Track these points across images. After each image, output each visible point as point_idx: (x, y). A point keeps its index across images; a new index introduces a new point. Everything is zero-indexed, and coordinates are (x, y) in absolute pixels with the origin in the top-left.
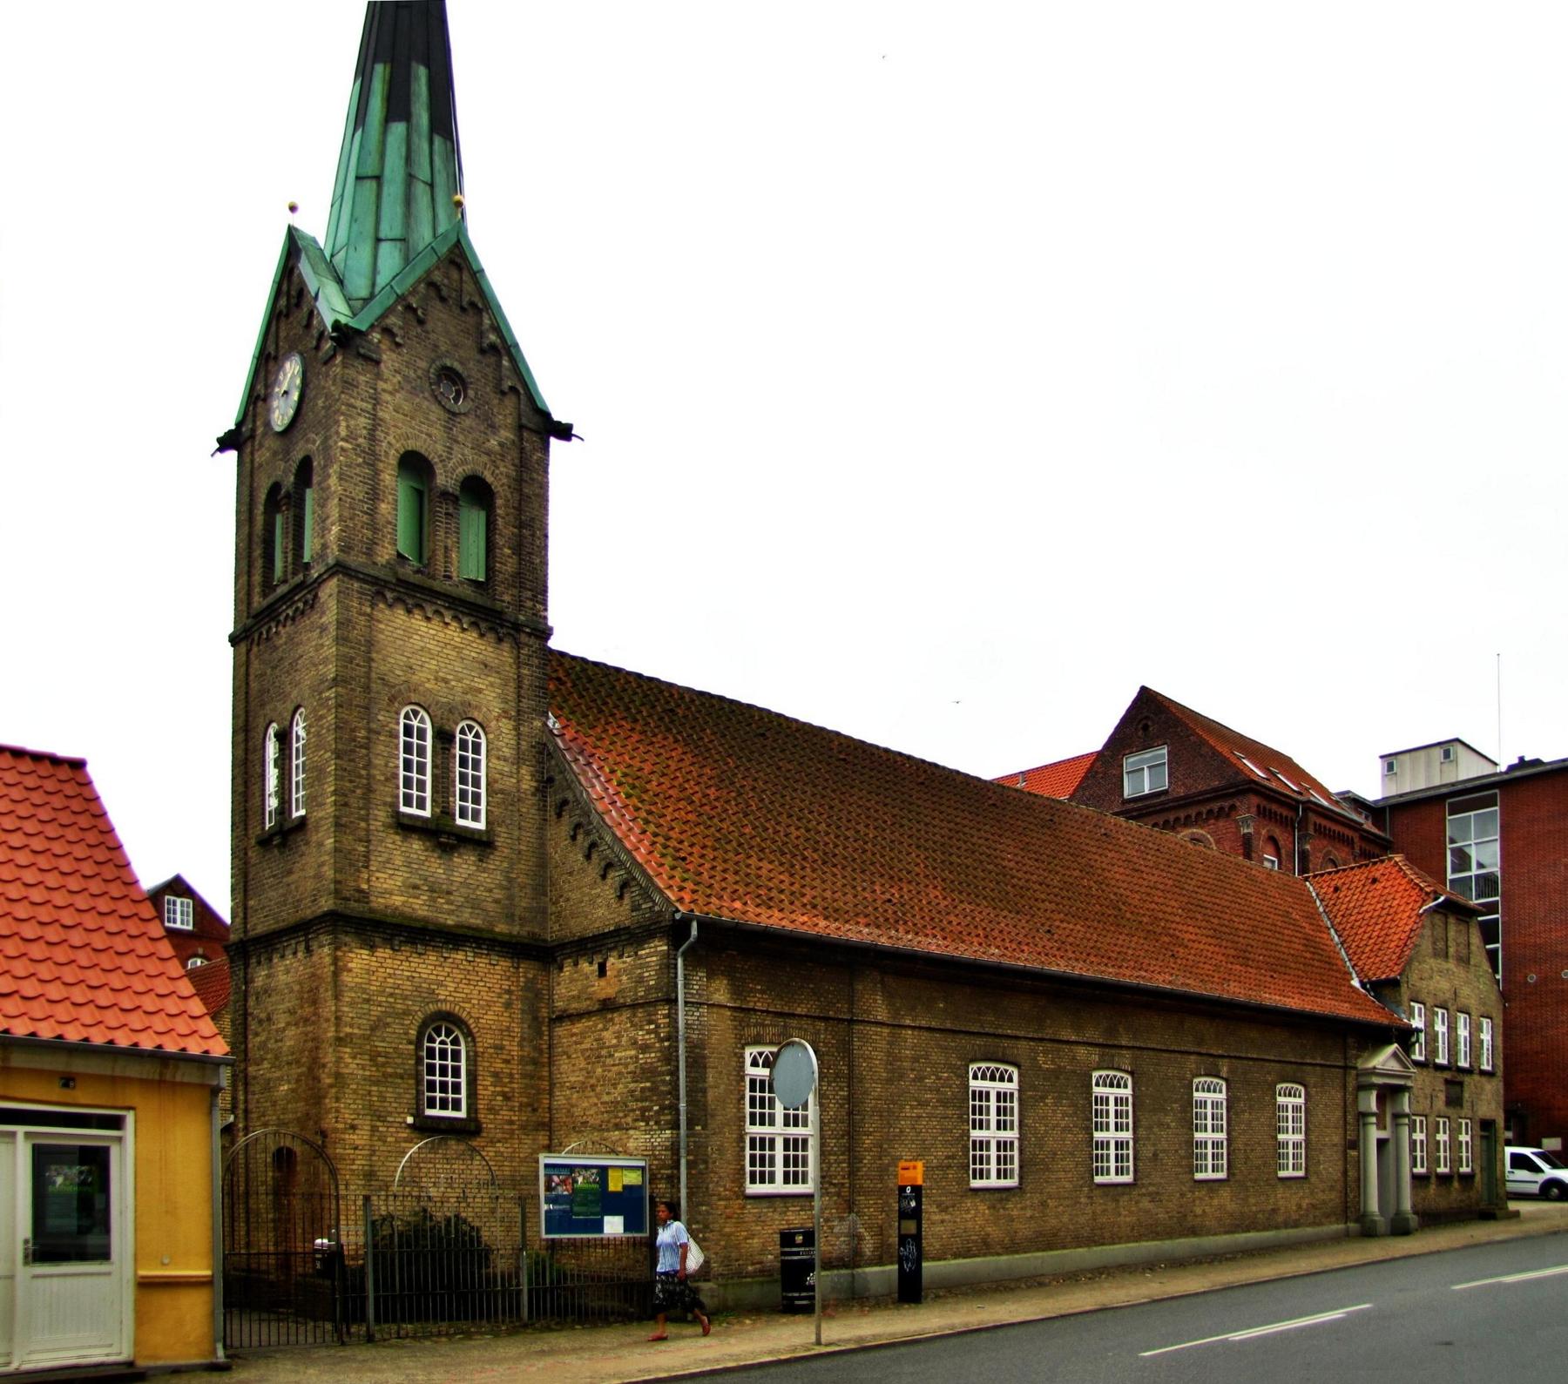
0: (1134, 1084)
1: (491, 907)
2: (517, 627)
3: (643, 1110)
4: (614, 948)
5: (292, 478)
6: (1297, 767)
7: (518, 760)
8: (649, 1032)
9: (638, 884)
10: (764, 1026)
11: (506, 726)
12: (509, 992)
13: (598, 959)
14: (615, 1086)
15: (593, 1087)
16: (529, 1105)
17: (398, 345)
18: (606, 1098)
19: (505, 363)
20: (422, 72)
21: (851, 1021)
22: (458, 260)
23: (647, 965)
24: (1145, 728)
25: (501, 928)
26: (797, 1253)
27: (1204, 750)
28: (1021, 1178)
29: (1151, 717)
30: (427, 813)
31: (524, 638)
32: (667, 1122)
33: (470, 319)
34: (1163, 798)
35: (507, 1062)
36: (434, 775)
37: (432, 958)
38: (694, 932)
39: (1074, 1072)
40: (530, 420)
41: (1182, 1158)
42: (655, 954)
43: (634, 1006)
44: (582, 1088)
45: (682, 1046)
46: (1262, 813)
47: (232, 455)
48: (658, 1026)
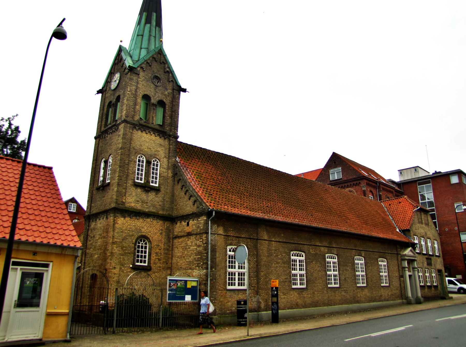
2: (170, 136)
3: (198, 264)
7: (168, 169)
8: (200, 242)
11: (165, 160)
12: (162, 230)
13: (187, 221)
14: (190, 257)
15: (184, 257)
21: (257, 239)
23: (201, 223)
24: (335, 162)
25: (161, 212)
26: (242, 307)
28: (307, 285)
29: (336, 160)
30: (143, 182)
32: (205, 268)
33: (163, 65)
35: (160, 249)
36: (145, 172)
37: (141, 220)
38: (214, 214)
39: (320, 254)
40: (176, 88)
43: (196, 234)
44: (181, 257)
46: (368, 185)
48: (203, 240)
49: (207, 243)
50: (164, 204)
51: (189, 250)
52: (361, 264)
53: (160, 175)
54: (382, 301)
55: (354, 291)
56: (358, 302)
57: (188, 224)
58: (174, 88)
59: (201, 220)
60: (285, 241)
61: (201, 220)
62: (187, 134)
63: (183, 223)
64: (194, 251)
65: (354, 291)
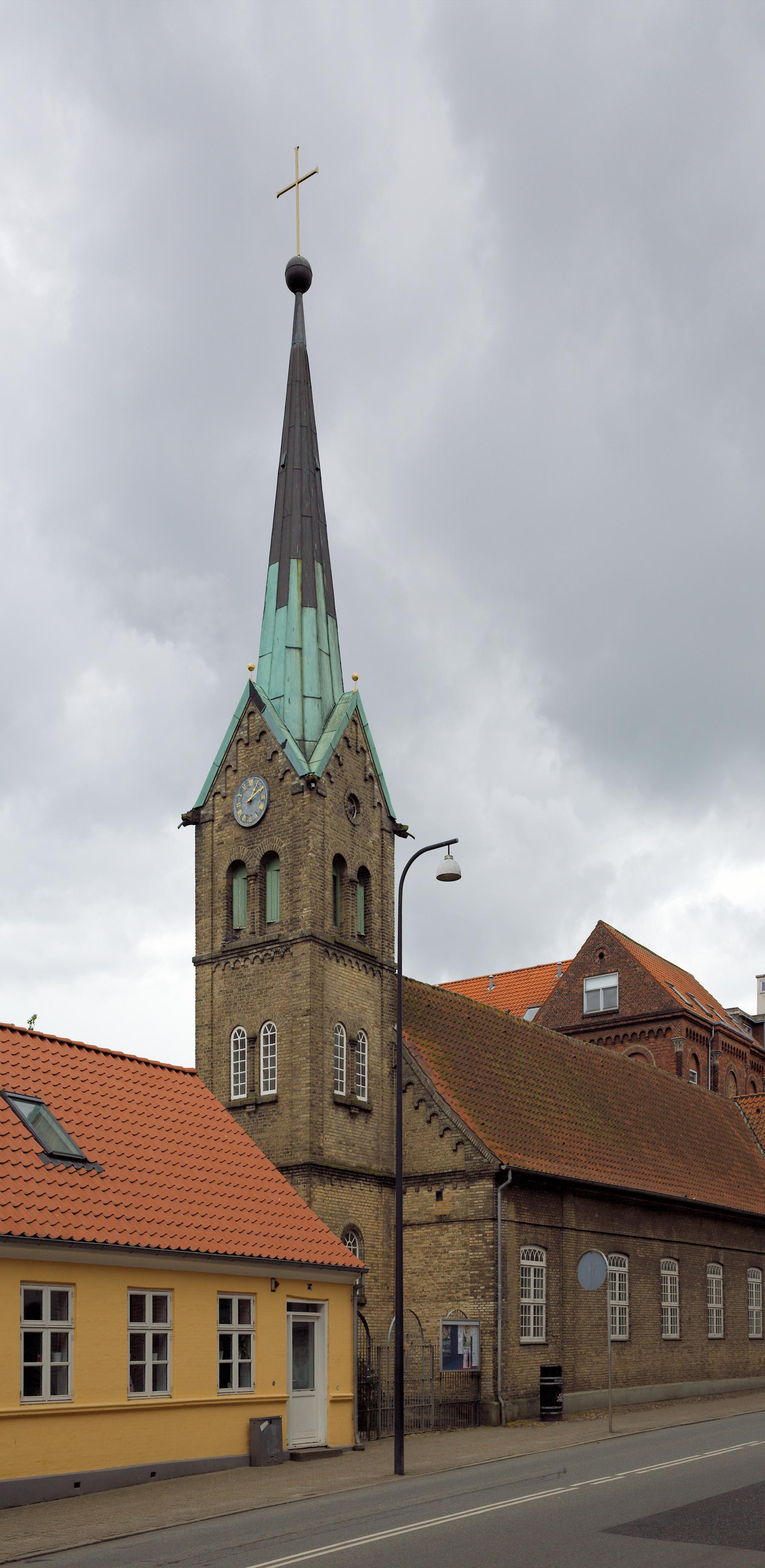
0: (679, 1267)
1: (370, 1152)
2: (382, 966)
3: (472, 1289)
4: (451, 1182)
5: (257, 863)
6: (697, 982)
7: (382, 1055)
8: (478, 1238)
9: (472, 1144)
10: (528, 1233)
11: (377, 1031)
12: (377, 1209)
13: (436, 1188)
14: (449, 1272)
15: (430, 1273)
16: (386, 1285)
17: (332, 782)
18: (441, 1280)
19: (376, 787)
20: (318, 567)
21: (562, 1228)
22: (356, 719)
23: (477, 1196)
24: (601, 956)
25: (375, 1167)
26: (553, 1381)
27: (647, 980)
28: (630, 1334)
29: (606, 948)
30: (343, 1094)
31: (385, 973)
32: (490, 1297)
33: (360, 758)
34: (614, 1016)
35: (376, 1256)
36: (347, 1068)
37: (347, 1188)
38: (510, 1177)
39: (652, 1259)
40: (387, 825)
41: (703, 1321)
42: (484, 1189)
43: (465, 1221)
44: (420, 1273)
45: (499, 1247)
46: (690, 1035)
47: (192, 828)
48: (485, 1235)
49: (495, 1243)
50: (378, 1146)
51: (445, 1256)
52: (538, 1272)
53: (369, 1072)
54: (749, 1376)
55: (703, 1349)
56: (708, 1376)
57: (439, 1196)
58: (384, 826)
59: (478, 1190)
60: (599, 1230)
61: (478, 1190)
62: (426, 963)
63: (424, 1192)
64: (458, 1259)
65: (703, 1349)
